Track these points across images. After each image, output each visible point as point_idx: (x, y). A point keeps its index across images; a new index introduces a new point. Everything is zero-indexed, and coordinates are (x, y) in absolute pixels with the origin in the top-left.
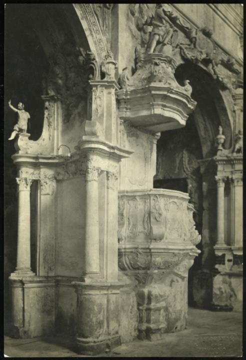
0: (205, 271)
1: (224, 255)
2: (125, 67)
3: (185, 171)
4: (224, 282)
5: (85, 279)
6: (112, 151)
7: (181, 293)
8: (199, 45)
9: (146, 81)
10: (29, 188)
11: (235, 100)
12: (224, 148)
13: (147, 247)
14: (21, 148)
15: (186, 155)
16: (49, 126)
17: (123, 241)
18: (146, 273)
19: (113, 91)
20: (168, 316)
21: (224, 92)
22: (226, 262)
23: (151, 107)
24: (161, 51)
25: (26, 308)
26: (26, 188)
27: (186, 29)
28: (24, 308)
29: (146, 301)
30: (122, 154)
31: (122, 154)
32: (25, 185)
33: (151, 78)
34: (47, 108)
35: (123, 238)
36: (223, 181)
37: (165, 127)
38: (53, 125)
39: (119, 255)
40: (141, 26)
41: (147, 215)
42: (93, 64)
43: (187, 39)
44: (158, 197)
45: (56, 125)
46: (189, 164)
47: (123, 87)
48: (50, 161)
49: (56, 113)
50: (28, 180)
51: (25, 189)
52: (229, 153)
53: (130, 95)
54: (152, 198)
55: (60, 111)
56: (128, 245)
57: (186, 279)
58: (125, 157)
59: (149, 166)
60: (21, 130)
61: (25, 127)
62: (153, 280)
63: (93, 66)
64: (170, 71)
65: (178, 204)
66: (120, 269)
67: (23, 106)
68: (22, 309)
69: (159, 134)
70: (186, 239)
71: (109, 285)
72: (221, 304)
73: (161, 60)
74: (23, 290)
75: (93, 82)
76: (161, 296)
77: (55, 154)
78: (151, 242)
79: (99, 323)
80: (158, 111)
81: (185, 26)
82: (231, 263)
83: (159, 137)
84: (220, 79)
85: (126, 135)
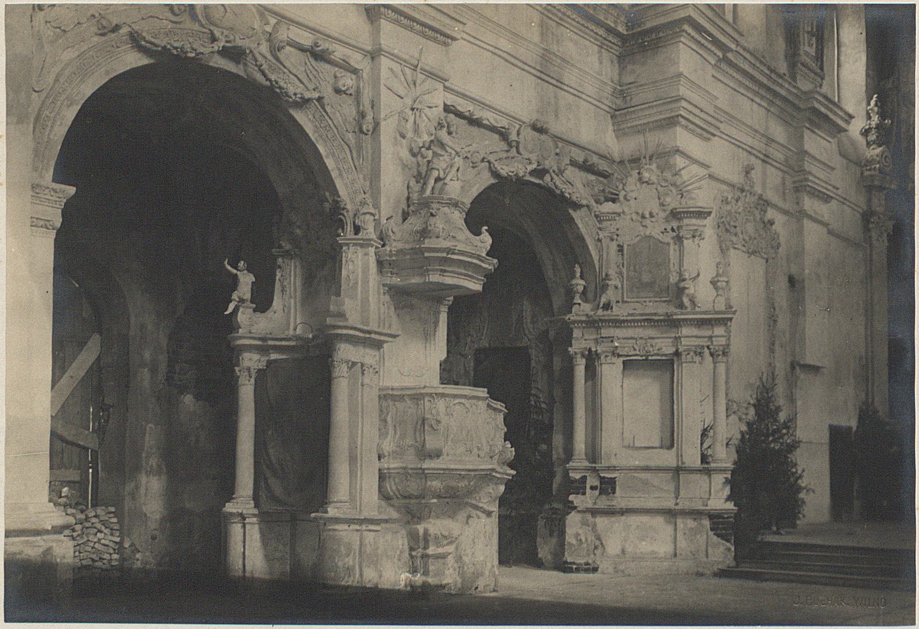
0: (555, 505)
1: (584, 478)
2: (389, 216)
3: (525, 335)
4: (584, 523)
5: (329, 509)
6: (367, 336)
7: (485, 537)
8: (525, 148)
9: (419, 235)
10: (253, 381)
11: (600, 222)
12: (586, 301)
13: (419, 466)
14: (242, 325)
15: (527, 307)
16: (282, 291)
17: (386, 458)
18: (420, 503)
19: (372, 250)
20: (463, 568)
21: (578, 212)
22: (588, 490)
23: (424, 273)
24: (442, 190)
25: (247, 553)
26: (249, 381)
27: (502, 129)
28: (244, 553)
29: (422, 544)
30: (382, 338)
31: (382, 338)
32: (248, 378)
33: (424, 233)
34: (280, 267)
35: (386, 454)
36: (583, 356)
37: (456, 292)
38: (288, 290)
39: (380, 478)
40: (416, 150)
41: (420, 423)
42: (344, 215)
43: (503, 143)
44: (435, 397)
45: (292, 289)
46: (533, 323)
47: (387, 242)
48: (284, 343)
49: (292, 273)
50: (251, 370)
51: (247, 382)
52: (592, 310)
53: (396, 255)
54: (426, 399)
55: (298, 271)
56: (393, 464)
57: (495, 515)
58: (387, 342)
59: (433, 347)
60: (242, 301)
61: (248, 296)
62: (433, 513)
63: (343, 218)
64: (458, 217)
65: (467, 405)
66: (382, 497)
67: (246, 265)
68: (241, 555)
69: (452, 298)
70: (482, 455)
71: (363, 518)
72: (578, 562)
73: (442, 203)
74: (244, 526)
75: (344, 240)
76: (445, 537)
77: (291, 332)
78: (425, 459)
79: (348, 569)
80: (435, 278)
81: (499, 126)
82: (597, 492)
83: (451, 302)
84: (567, 195)
85: (393, 308)
